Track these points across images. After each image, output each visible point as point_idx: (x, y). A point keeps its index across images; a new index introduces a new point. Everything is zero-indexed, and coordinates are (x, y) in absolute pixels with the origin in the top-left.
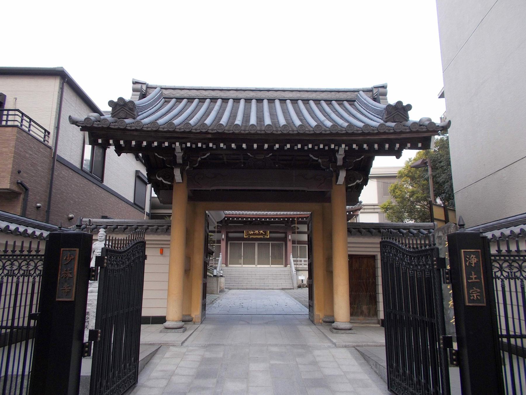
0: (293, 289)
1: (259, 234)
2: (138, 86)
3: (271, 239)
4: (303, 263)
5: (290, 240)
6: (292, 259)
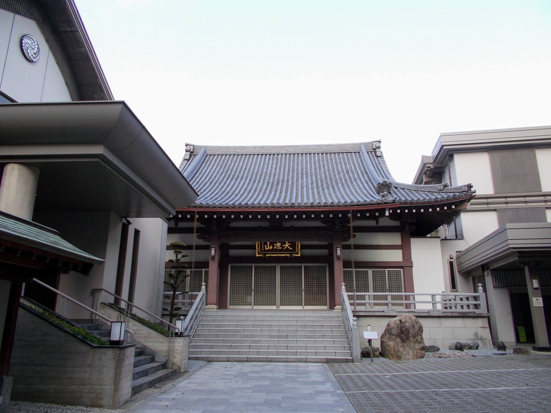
0: (352, 361)
1: (282, 250)
2: (188, 148)
3: (304, 259)
4: (367, 301)
5: (338, 258)
6: (345, 295)
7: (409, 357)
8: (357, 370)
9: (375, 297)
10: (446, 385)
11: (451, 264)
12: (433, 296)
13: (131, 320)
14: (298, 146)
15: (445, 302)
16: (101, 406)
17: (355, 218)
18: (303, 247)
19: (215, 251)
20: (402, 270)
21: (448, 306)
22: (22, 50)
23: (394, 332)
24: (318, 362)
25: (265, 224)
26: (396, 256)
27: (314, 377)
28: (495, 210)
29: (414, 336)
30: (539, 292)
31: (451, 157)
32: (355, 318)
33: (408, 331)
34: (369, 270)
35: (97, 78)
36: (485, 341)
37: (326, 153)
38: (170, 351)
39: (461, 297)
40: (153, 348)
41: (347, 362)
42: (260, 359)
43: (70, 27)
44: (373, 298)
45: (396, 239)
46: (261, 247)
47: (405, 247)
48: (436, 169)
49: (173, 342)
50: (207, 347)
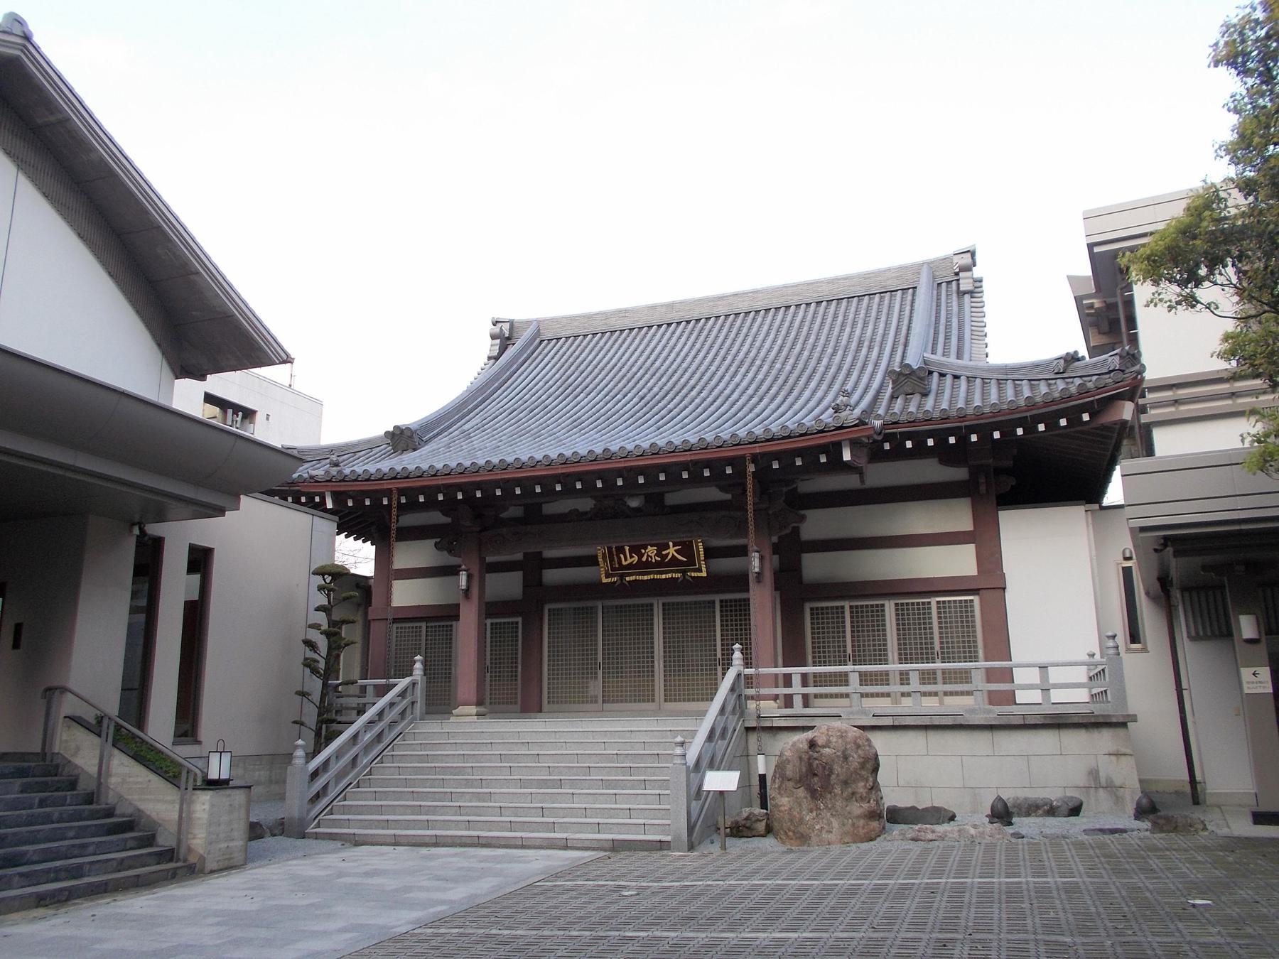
1: (663, 564)
2: (497, 329)
7: (831, 837)
11: (1127, 573)
13: (116, 752)
14: (757, 292)
18: (711, 553)
19: (762, 559)
20: (976, 599)
24: (594, 849)
25: (586, 504)
26: (959, 562)
28: (1253, 412)
29: (846, 783)
30: (1262, 650)
33: (828, 769)
34: (886, 603)
35: (147, 212)
38: (184, 820)
40: (154, 815)
41: (661, 849)
42: (464, 840)
44: (891, 676)
45: (958, 516)
46: (612, 561)
47: (985, 540)
49: (191, 802)
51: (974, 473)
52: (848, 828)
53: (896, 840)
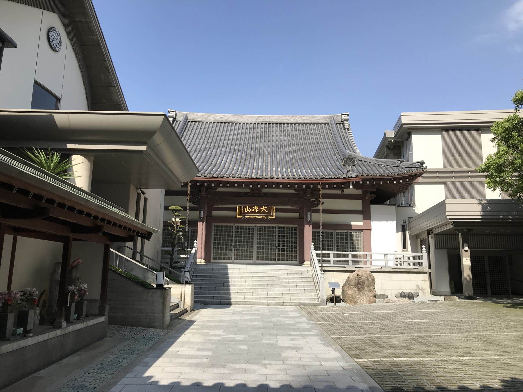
8: (324, 311)
9: (338, 256)
10: (387, 319)
12: (385, 255)
15: (397, 260)
16: (154, 327)
17: (324, 188)
18: (277, 210)
21: (398, 263)
22: (49, 42)
23: (352, 283)
25: (247, 190)
27: (292, 314)
28: (443, 183)
29: (368, 287)
31: (409, 135)
32: (322, 272)
35: (105, 61)
36: (425, 291)
37: (299, 124)
39: (409, 256)
43: (85, 18)
45: (358, 205)
46: (241, 210)
48: (397, 145)
50: (203, 293)
51: (365, 193)
52: (368, 299)
53: (379, 302)
